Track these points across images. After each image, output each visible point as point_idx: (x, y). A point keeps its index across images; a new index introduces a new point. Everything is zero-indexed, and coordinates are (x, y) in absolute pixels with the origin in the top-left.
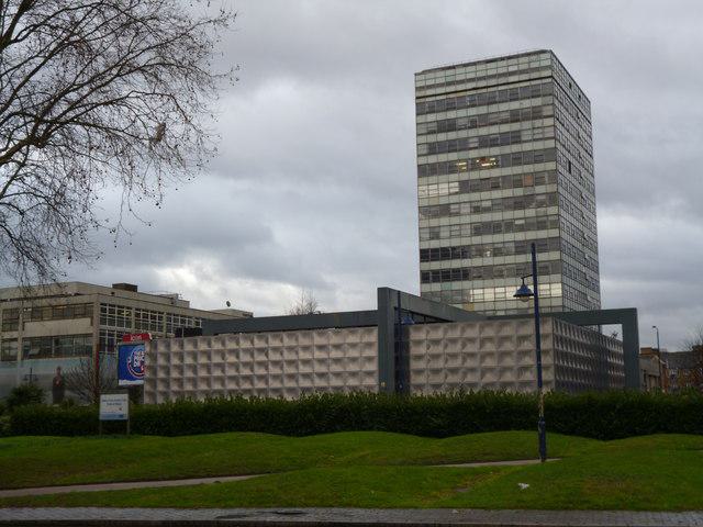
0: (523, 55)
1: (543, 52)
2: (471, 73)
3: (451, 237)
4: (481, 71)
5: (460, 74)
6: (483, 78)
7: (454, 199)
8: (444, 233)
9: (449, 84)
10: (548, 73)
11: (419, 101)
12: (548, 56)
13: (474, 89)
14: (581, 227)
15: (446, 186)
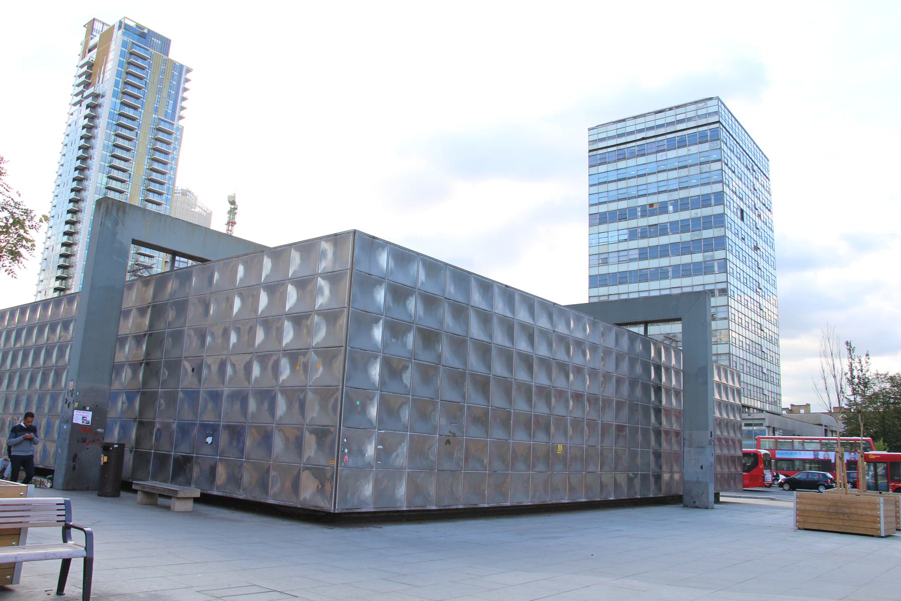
0: (691, 104)
1: (711, 99)
2: (641, 124)
3: (619, 262)
4: (651, 121)
5: (630, 126)
6: (652, 128)
7: (623, 246)
8: (613, 258)
9: (619, 136)
10: (715, 119)
11: (591, 153)
12: (715, 102)
13: (643, 139)
14: (759, 319)
15: (616, 233)
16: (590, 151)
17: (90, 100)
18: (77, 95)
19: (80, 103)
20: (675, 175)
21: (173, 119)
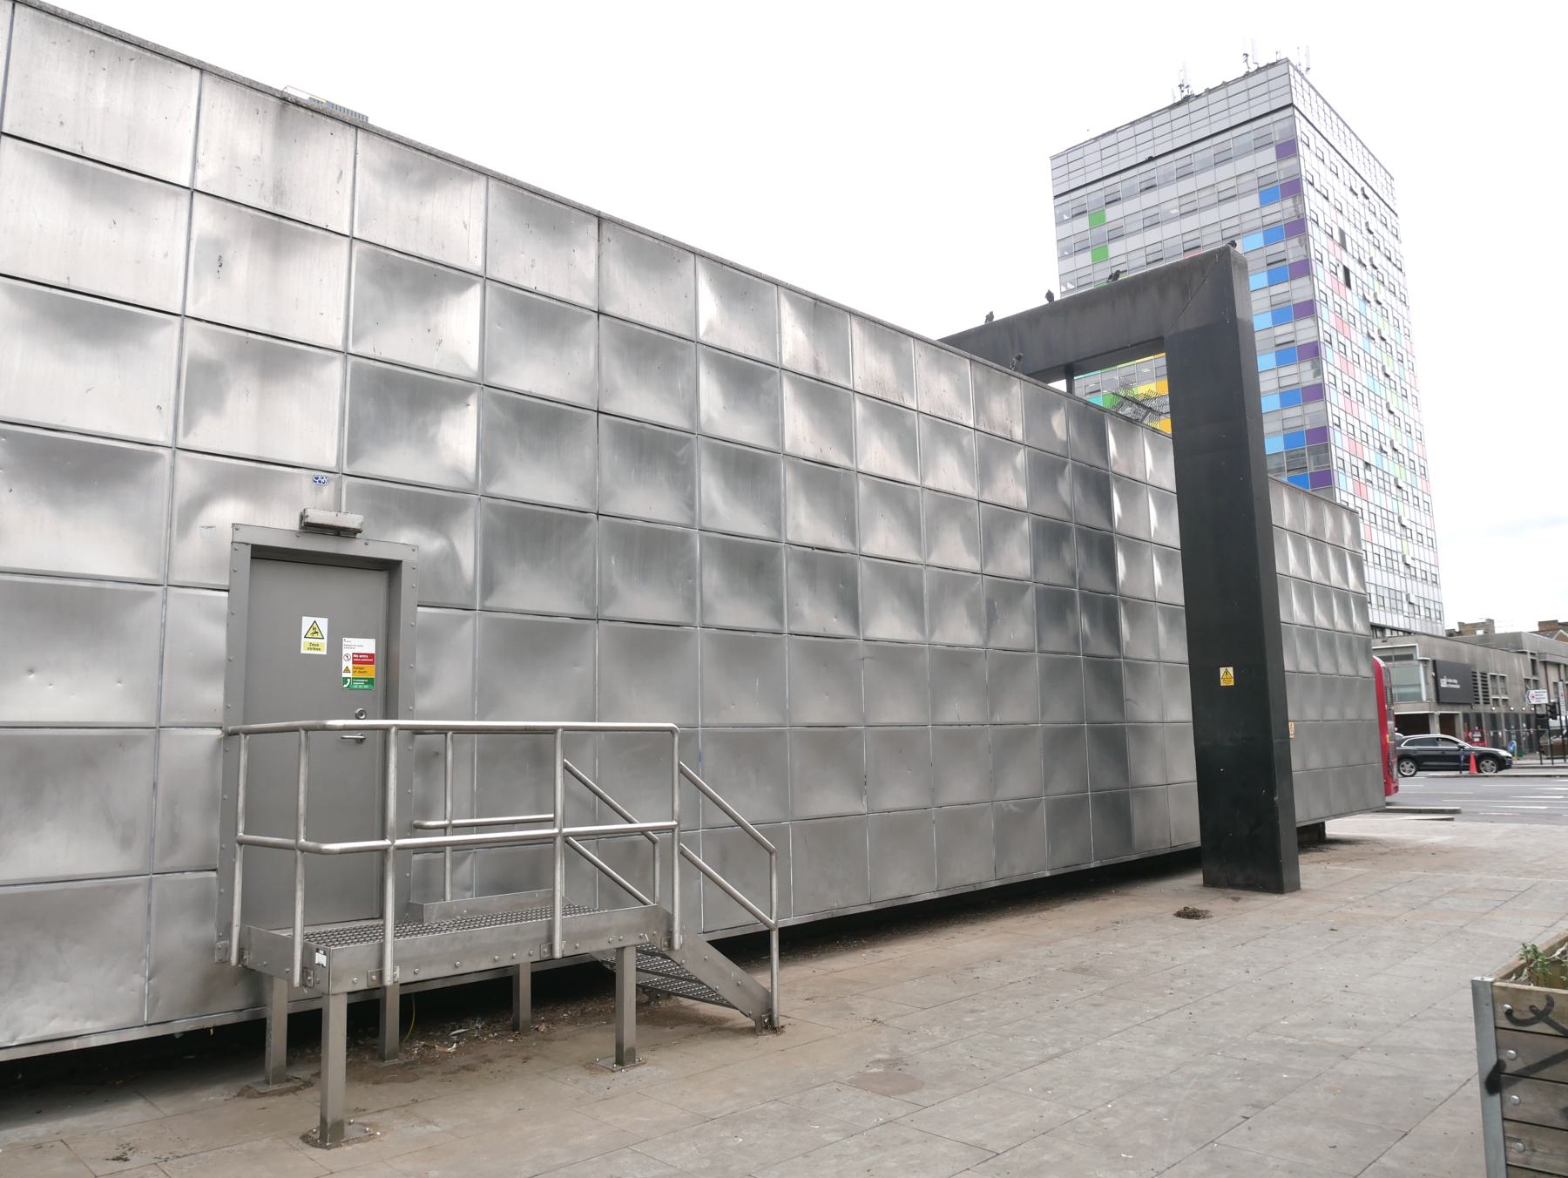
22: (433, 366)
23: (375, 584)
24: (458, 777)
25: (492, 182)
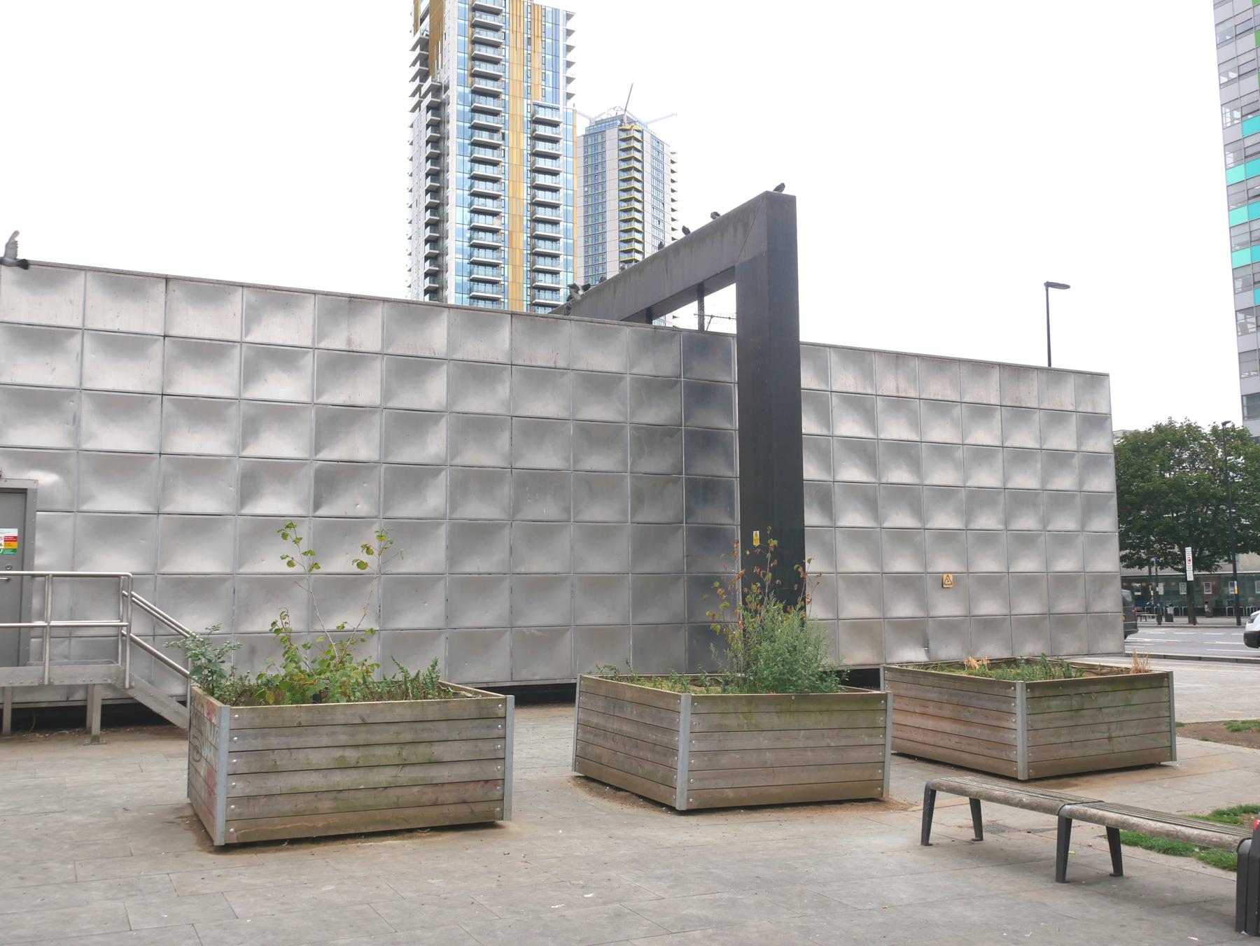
16: (1217, 25)
17: (429, 98)
18: (413, 95)
19: (418, 105)
20: (715, 215)
21: (556, 99)
22: (49, 384)
23: (16, 500)
24: (62, 597)
25: (89, 274)
